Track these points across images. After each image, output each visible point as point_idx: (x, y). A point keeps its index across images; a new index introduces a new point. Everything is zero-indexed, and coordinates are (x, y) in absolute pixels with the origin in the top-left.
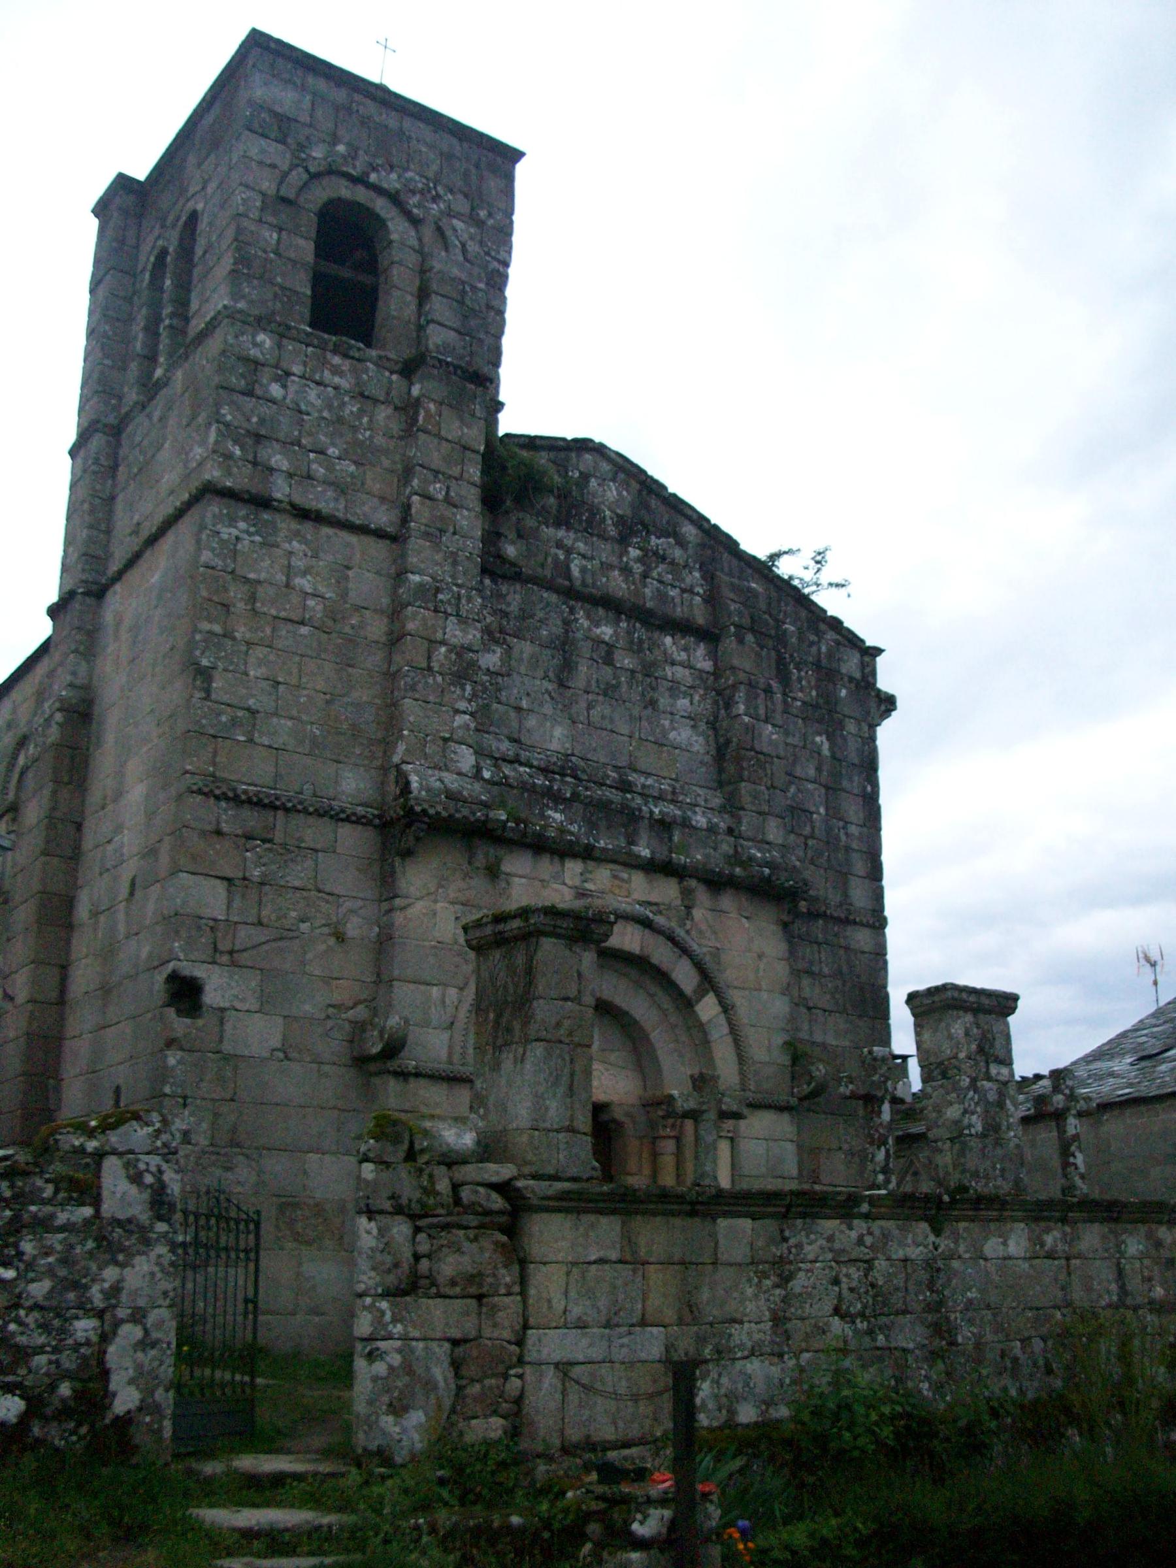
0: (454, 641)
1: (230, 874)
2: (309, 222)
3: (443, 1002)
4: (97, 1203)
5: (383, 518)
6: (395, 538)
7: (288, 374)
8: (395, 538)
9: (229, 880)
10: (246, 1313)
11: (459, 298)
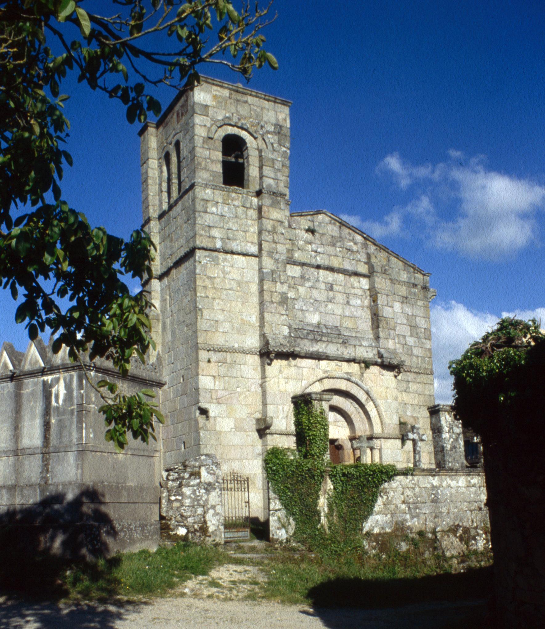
0: (279, 291)
1: (214, 375)
2: (219, 145)
3: (283, 411)
4: (200, 478)
5: (254, 249)
6: (258, 256)
7: (217, 203)
8: (258, 256)
9: (214, 377)
10: (246, 506)
11: (272, 165)
